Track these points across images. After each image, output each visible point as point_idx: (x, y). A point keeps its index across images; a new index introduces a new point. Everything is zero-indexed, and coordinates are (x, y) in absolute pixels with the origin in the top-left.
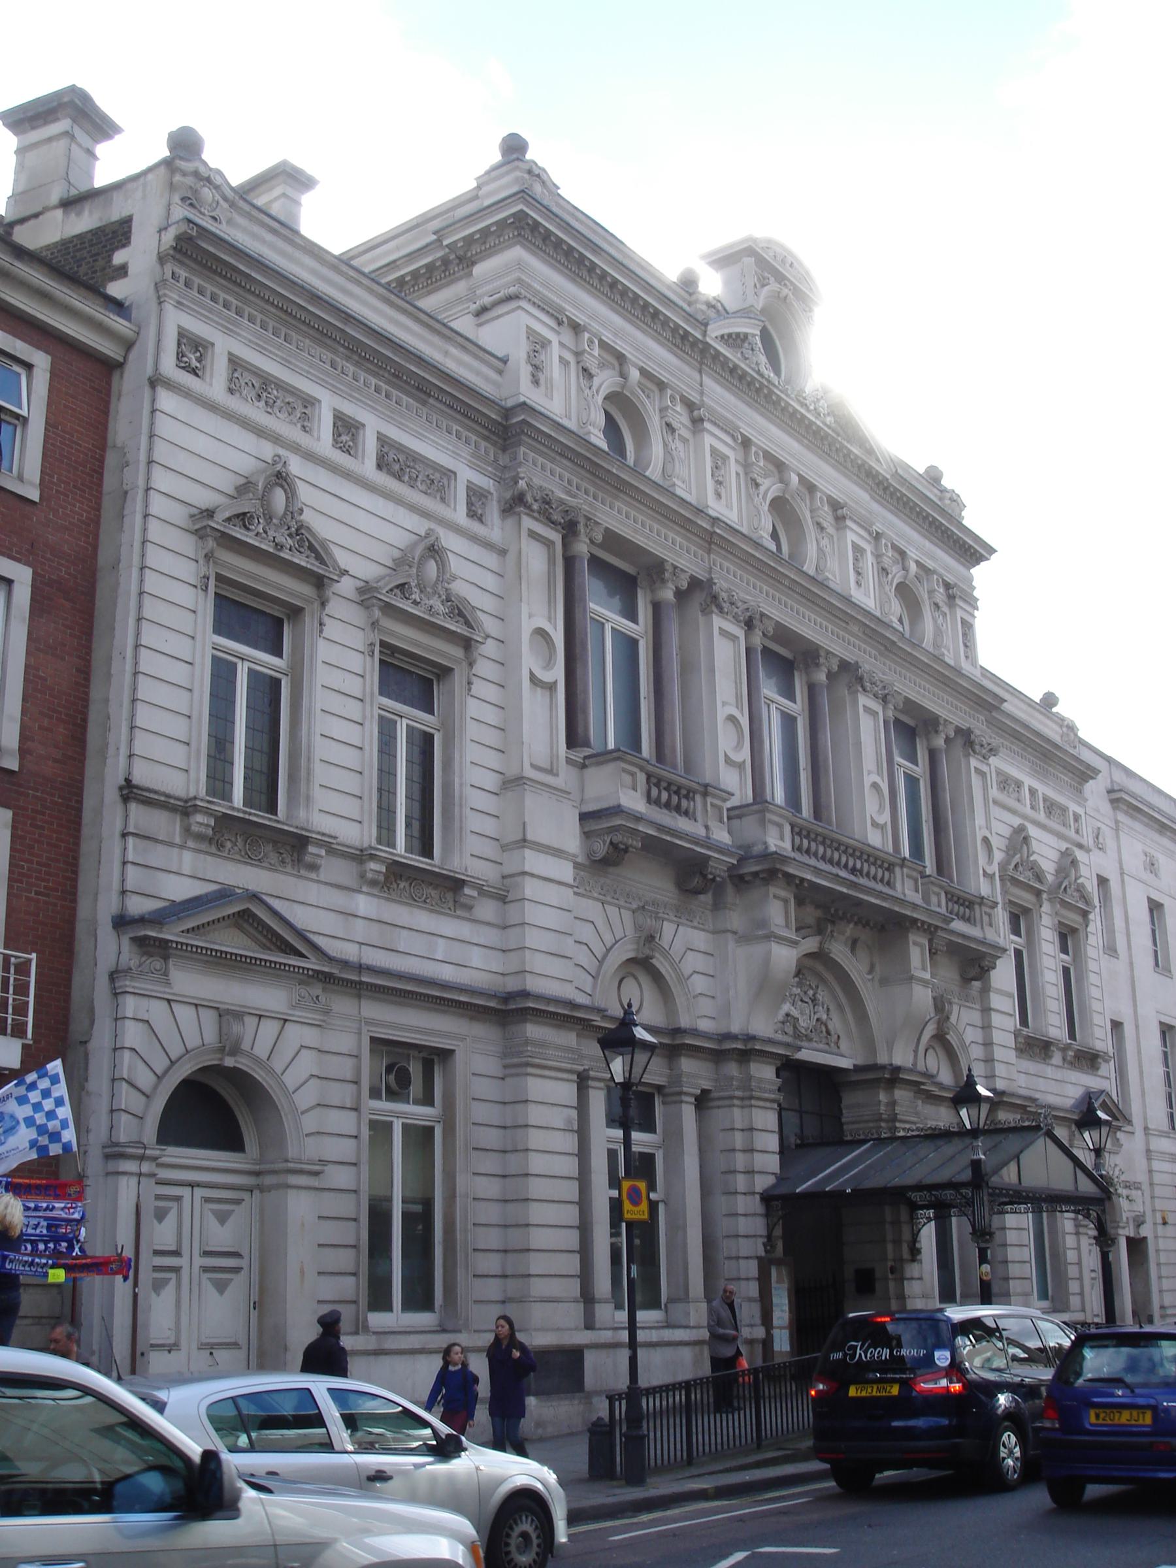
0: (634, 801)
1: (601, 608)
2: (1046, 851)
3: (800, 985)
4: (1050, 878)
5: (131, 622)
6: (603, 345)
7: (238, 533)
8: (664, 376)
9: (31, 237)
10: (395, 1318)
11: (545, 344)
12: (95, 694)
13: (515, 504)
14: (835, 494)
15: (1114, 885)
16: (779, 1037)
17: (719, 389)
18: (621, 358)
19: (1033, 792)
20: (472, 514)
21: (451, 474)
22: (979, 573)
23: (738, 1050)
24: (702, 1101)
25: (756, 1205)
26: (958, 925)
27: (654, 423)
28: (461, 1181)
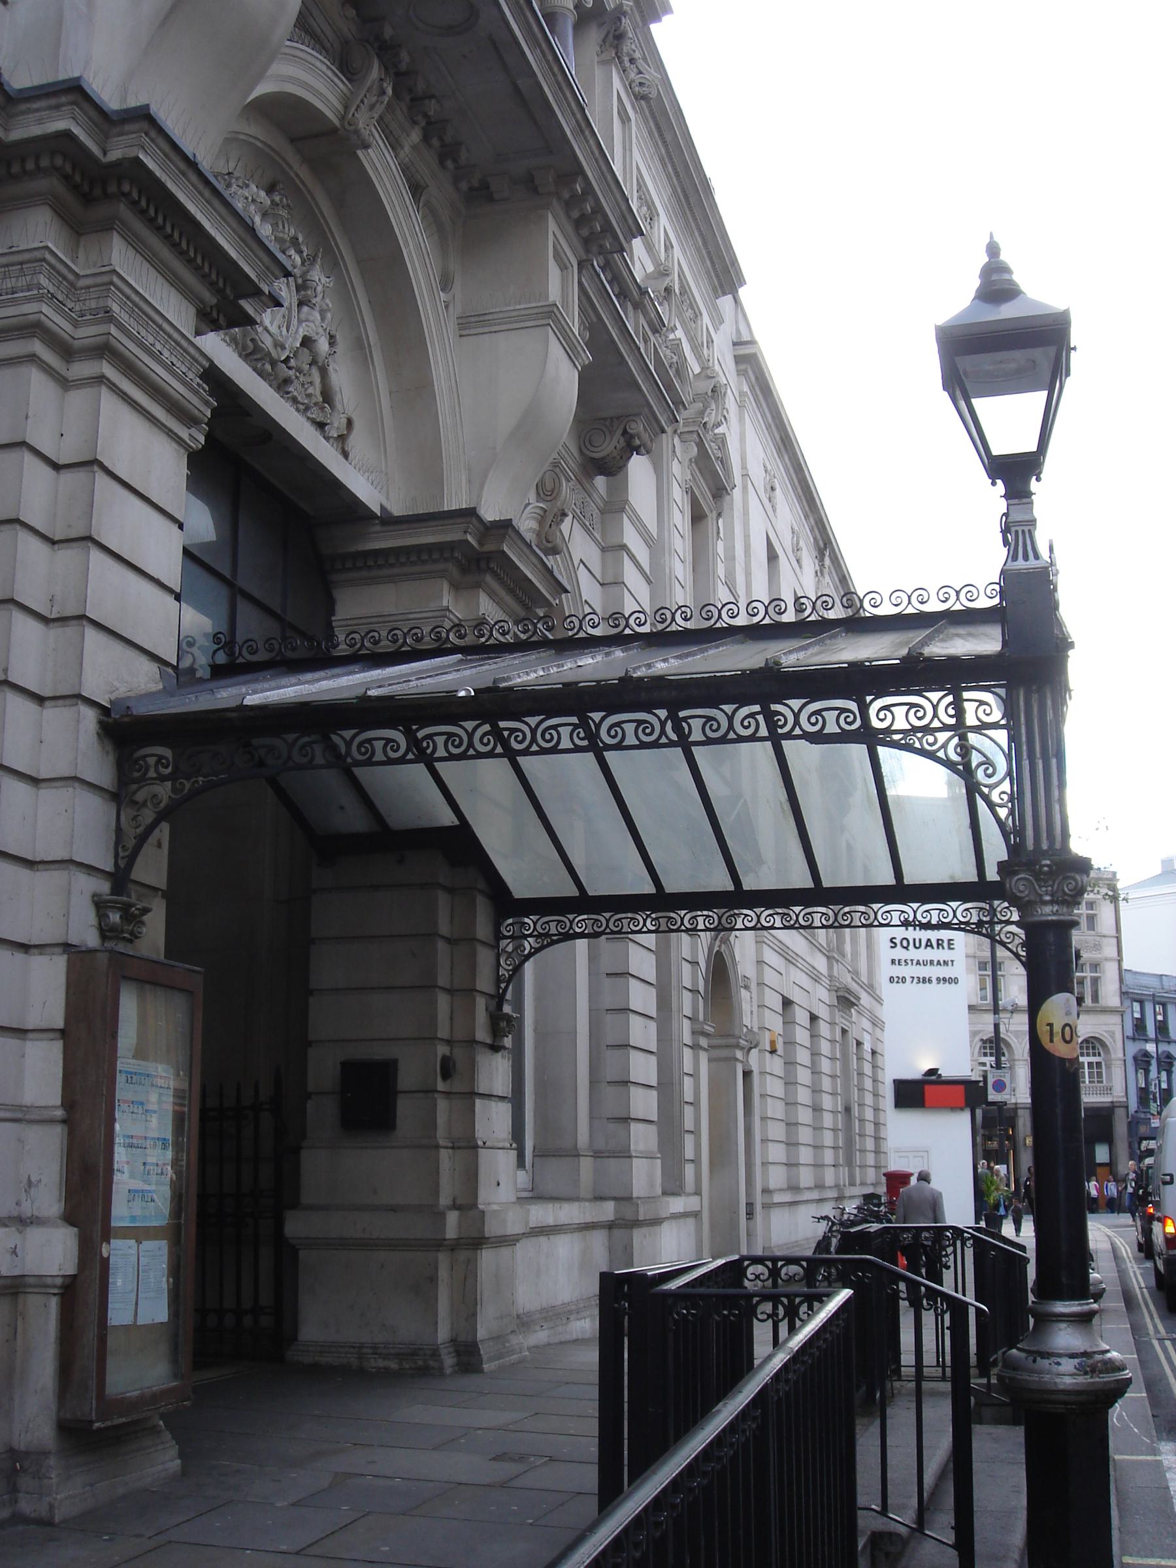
25: (74, 743)
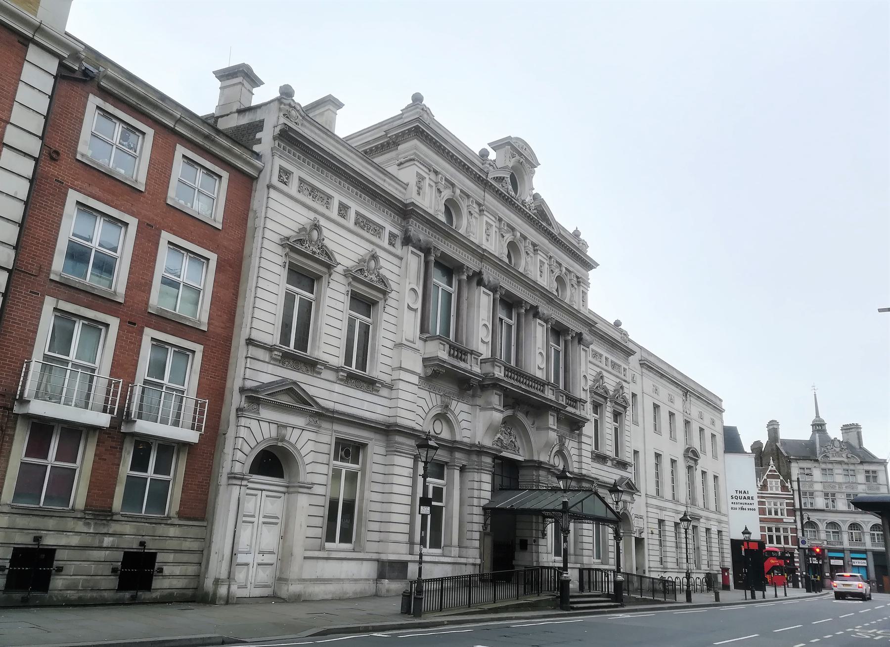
0: (443, 354)
1: (438, 279)
2: (610, 383)
3: (504, 427)
4: (611, 393)
5: (255, 278)
6: (446, 180)
7: (298, 246)
8: (470, 193)
9: (222, 125)
10: (337, 545)
11: (423, 178)
12: (240, 303)
13: (407, 241)
14: (534, 241)
15: (639, 397)
16: (495, 446)
17: (491, 198)
18: (453, 185)
19: (606, 359)
20: (390, 244)
21: (383, 228)
22: (592, 273)
23: (479, 451)
24: (463, 469)
25: (478, 511)
26: (569, 409)
27: (465, 211)
28: (366, 493)
